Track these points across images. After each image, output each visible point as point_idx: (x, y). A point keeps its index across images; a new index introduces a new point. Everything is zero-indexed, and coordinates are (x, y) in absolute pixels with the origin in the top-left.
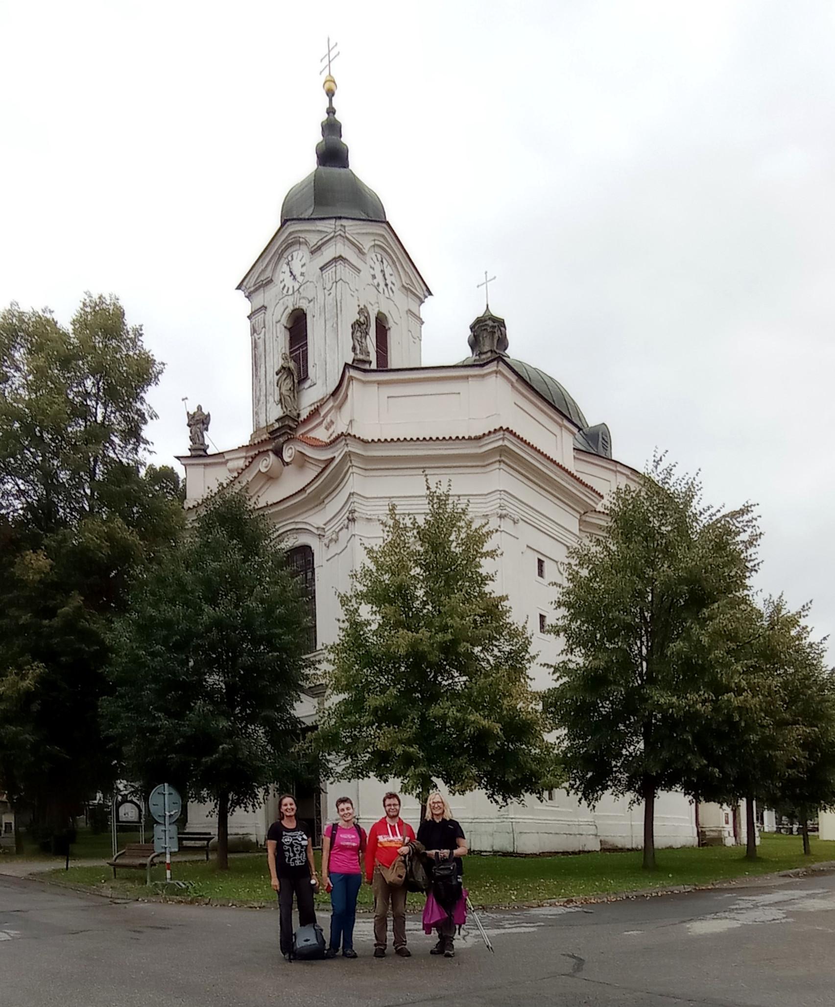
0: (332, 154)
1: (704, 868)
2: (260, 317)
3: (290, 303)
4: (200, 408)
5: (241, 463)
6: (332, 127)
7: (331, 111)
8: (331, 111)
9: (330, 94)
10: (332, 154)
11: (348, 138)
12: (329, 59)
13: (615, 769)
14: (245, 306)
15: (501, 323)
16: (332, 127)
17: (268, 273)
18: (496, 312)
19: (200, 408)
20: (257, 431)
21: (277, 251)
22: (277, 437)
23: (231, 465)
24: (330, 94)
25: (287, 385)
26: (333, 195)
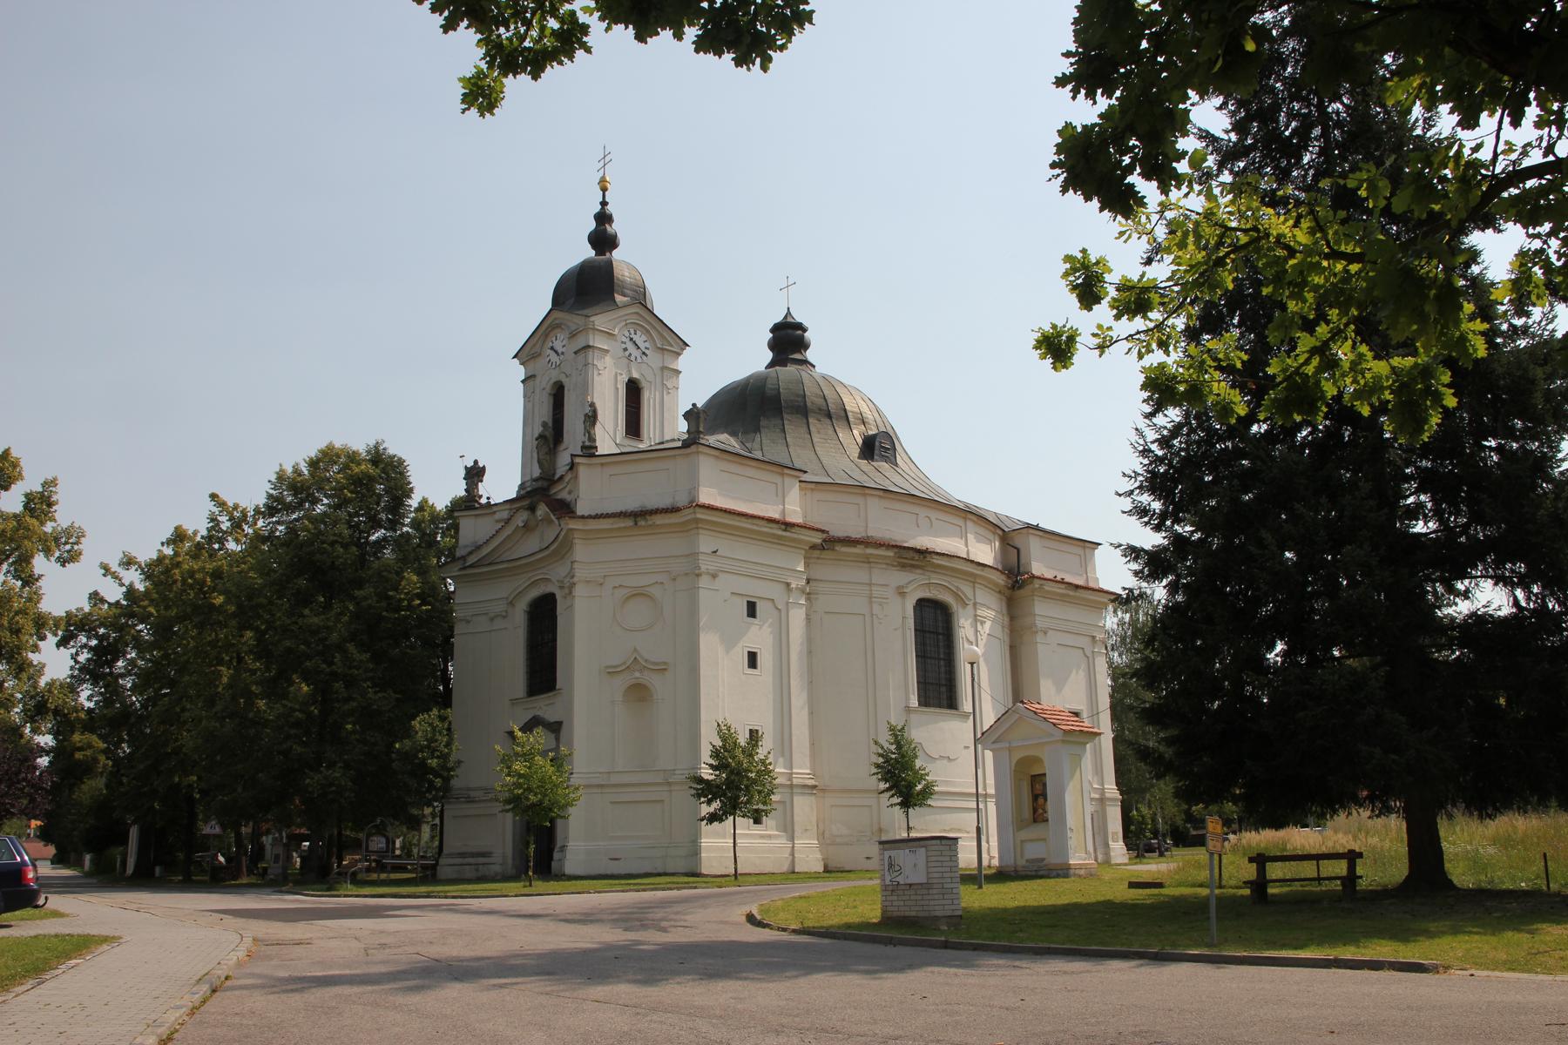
0: (603, 240)
1: (951, 830)
2: (531, 383)
3: (555, 376)
4: (476, 462)
5: (505, 515)
6: (603, 218)
7: (604, 203)
8: (604, 203)
9: (604, 190)
10: (603, 240)
11: (617, 227)
12: (605, 160)
13: (1362, 382)
14: (520, 372)
15: (801, 328)
16: (603, 218)
17: (537, 349)
18: (798, 317)
19: (476, 462)
20: (522, 487)
21: (544, 330)
22: (544, 493)
23: (497, 516)
24: (604, 190)
25: (545, 449)
26: (590, 287)
